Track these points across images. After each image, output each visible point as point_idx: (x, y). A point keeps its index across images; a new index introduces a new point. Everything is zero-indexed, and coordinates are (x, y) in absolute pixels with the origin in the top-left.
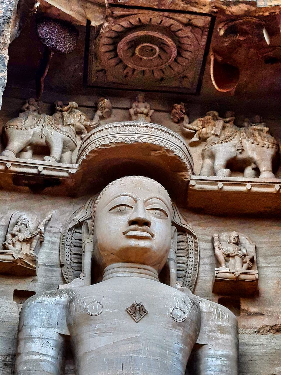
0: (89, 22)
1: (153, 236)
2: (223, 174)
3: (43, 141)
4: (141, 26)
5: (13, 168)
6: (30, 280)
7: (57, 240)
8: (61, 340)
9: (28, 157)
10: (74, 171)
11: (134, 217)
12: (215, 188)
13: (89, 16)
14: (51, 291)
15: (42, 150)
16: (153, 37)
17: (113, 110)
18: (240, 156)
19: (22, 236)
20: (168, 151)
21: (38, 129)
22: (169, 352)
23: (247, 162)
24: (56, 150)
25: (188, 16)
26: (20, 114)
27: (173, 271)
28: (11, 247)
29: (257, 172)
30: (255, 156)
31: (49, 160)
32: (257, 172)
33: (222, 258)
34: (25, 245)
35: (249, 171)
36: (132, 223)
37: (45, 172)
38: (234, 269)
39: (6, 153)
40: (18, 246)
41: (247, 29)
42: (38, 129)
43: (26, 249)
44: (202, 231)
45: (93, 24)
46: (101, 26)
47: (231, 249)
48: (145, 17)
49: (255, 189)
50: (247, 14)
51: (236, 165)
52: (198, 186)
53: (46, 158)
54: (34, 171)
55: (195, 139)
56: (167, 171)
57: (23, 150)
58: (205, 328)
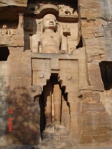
2: (65, 14)
3: (33, 8)
9: (30, 10)
11: (50, 21)
12: (63, 16)
14: (102, 135)
16: (48, 9)
17: (40, 52)
23: (69, 12)
26: (55, 86)
29: (70, 14)
30: (70, 11)
32: (70, 14)
33: (64, 29)
35: (69, 13)
36: (50, 22)
38: (66, 31)
41: (4, 112)
42: (32, 6)
44: (61, 24)
47: (66, 27)
51: (66, 12)
52: (61, 16)
55: (59, 8)
56: (55, 13)
57: (30, 9)
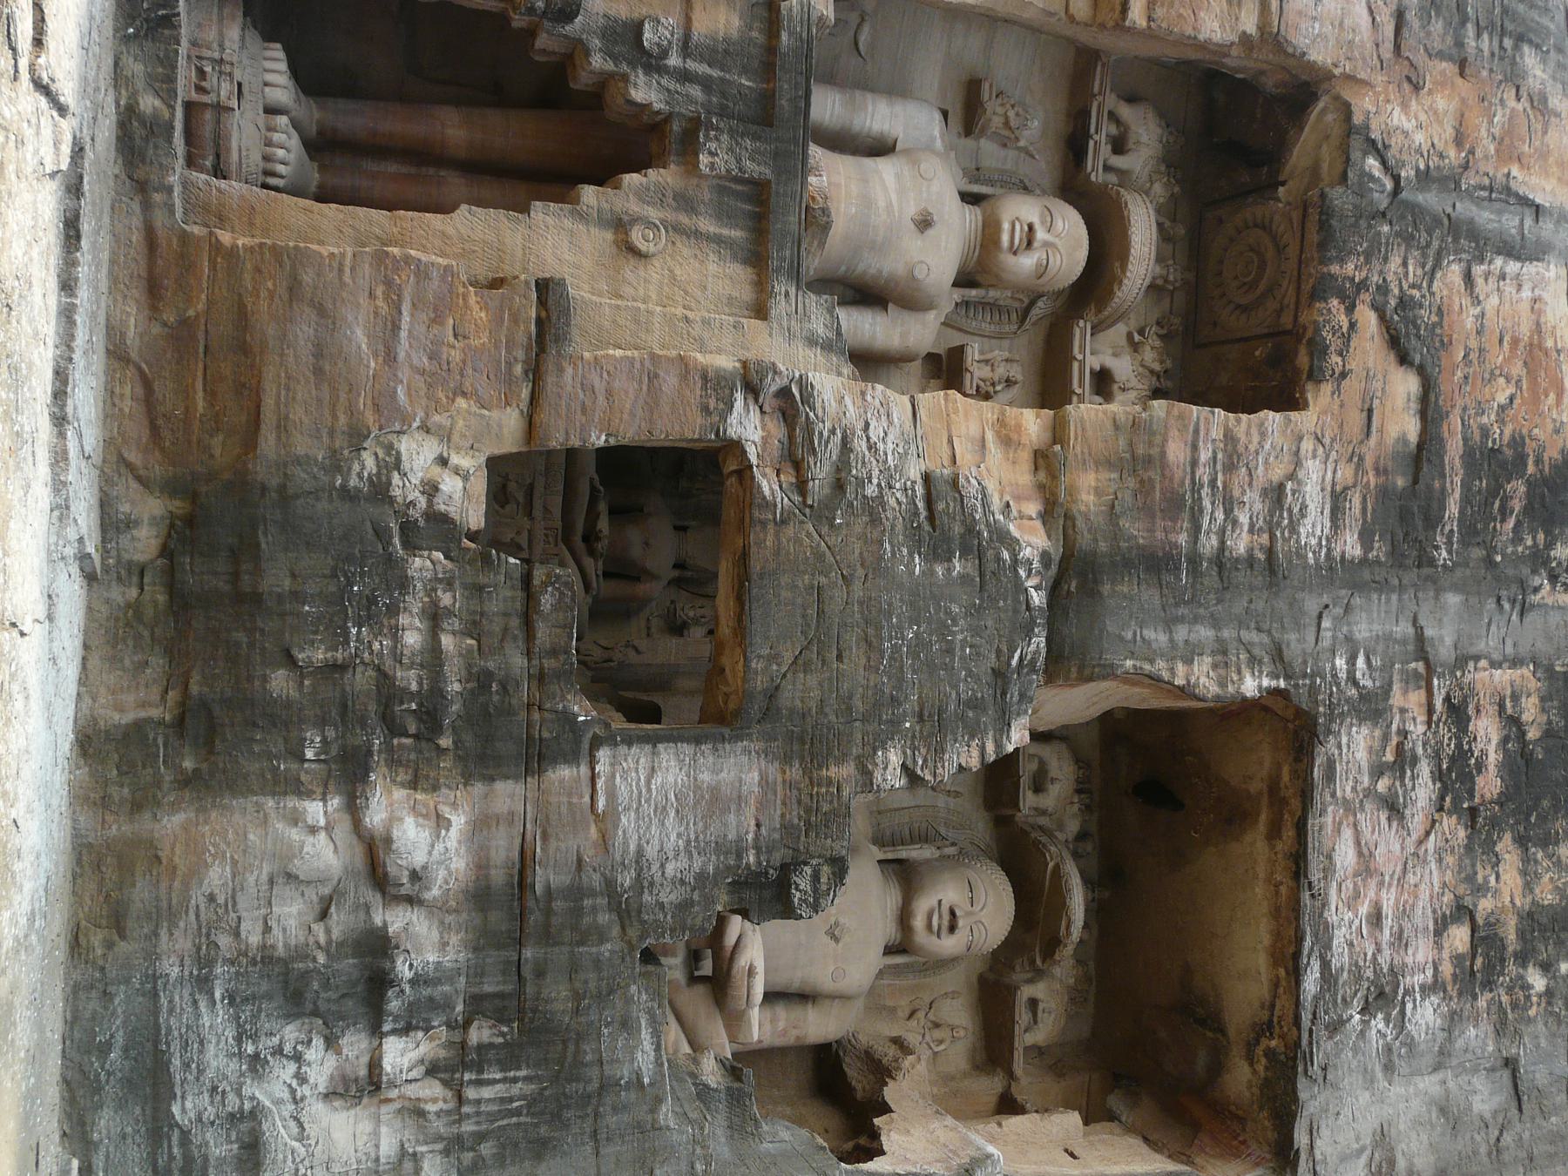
0: (1283, 184)
1: (1015, 253)
2: (1093, 362)
3: (1131, 145)
4: (1280, 250)
5: (1095, 104)
6: (961, 130)
7: (1008, 166)
8: (890, 142)
10: (1093, 178)
13: (1291, 183)
15: (1119, 146)
18: (1115, 387)
19: (1011, 114)
20: (1121, 282)
21: (1145, 139)
22: (920, 643)
24: (1118, 161)
25: (1292, 306)
27: (973, 293)
28: (999, 101)
31: (1106, 149)
34: (1002, 120)
36: (1031, 227)
37: (1091, 143)
39: (1113, 96)
40: (1000, 110)
43: (997, 121)
45: (1281, 189)
46: (1278, 200)
48: (1292, 251)
49: (1076, 365)
50: (1297, 371)
52: (1077, 332)
53: (1109, 147)
54: (1092, 130)
55: (1137, 337)
56: (1093, 285)
58: (906, 315)
